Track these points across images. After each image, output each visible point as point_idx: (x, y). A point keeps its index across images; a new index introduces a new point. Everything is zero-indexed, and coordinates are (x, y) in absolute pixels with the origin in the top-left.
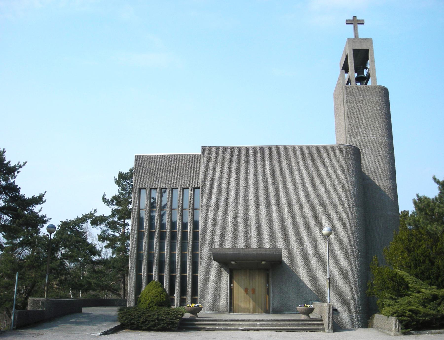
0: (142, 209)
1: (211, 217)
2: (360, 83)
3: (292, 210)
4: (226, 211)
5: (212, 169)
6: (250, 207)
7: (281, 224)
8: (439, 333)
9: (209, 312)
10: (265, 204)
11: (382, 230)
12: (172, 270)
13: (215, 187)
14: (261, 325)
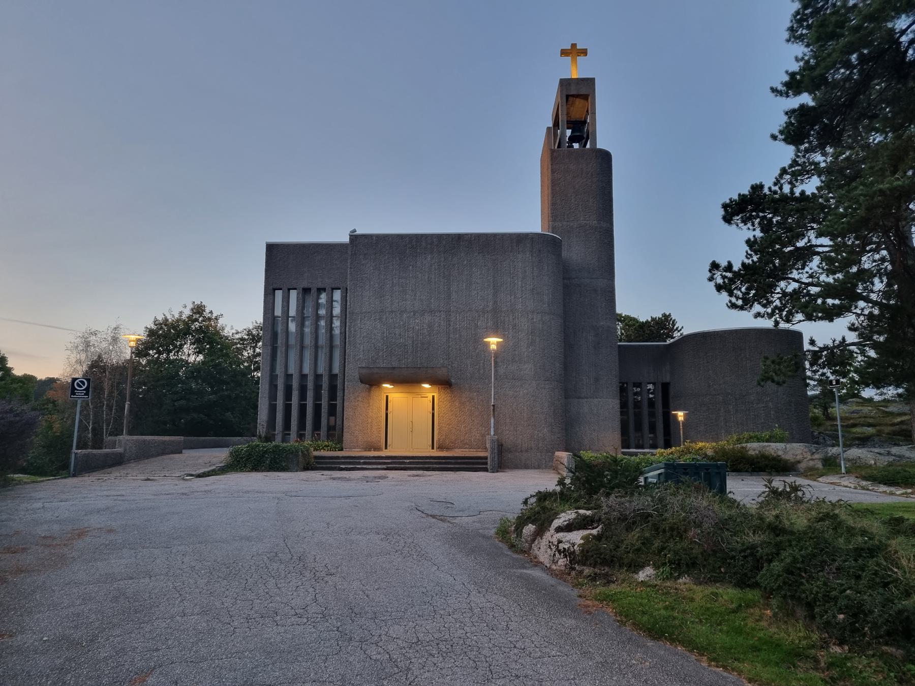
0: (335, 301)
4: (380, 319)
5: (363, 265)
6: (412, 314)
7: (452, 336)
10: (431, 312)
12: (318, 396)
14: (410, 463)
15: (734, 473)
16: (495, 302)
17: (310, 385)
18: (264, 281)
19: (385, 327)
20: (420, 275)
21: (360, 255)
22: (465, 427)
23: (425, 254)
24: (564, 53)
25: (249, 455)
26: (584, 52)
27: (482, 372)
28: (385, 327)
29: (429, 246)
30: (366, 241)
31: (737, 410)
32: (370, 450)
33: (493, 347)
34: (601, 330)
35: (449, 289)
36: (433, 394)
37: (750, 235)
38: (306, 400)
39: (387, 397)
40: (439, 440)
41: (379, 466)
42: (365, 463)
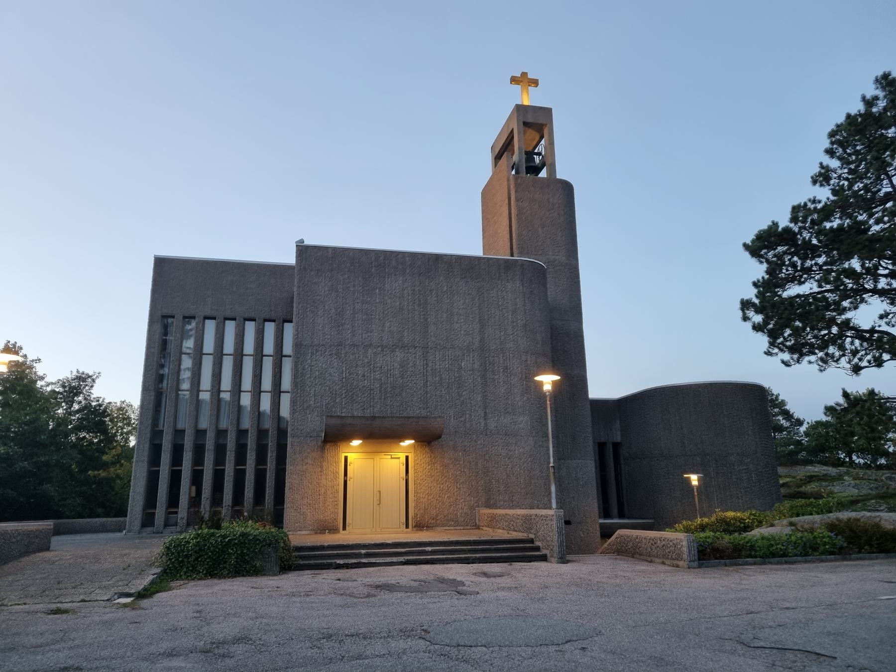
1: (312, 364)
2: (514, 174)
3: (447, 357)
5: (315, 283)
6: (380, 349)
7: (430, 378)
8: (855, 565)
9: (303, 532)
10: (403, 347)
11: (567, 397)
13: (320, 313)
15: (883, 555)
16: (482, 339)
17: (210, 444)
18: (149, 306)
19: (344, 365)
20: (389, 301)
21: (311, 270)
22: (449, 497)
23: (395, 275)
24: (514, 80)
25: (200, 550)
26: (535, 83)
27: (468, 425)
28: (344, 365)
29: (400, 267)
30: (320, 254)
31: (717, 473)
32: (322, 532)
33: (547, 387)
34: (575, 379)
35: (426, 320)
36: (407, 454)
37: (764, 276)
38: (244, 464)
39: (346, 458)
40: (416, 515)
41: (395, 559)
42: (368, 555)
